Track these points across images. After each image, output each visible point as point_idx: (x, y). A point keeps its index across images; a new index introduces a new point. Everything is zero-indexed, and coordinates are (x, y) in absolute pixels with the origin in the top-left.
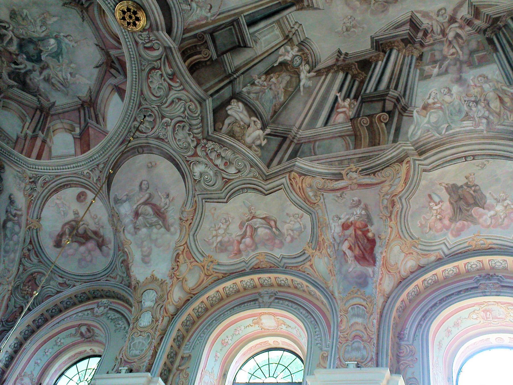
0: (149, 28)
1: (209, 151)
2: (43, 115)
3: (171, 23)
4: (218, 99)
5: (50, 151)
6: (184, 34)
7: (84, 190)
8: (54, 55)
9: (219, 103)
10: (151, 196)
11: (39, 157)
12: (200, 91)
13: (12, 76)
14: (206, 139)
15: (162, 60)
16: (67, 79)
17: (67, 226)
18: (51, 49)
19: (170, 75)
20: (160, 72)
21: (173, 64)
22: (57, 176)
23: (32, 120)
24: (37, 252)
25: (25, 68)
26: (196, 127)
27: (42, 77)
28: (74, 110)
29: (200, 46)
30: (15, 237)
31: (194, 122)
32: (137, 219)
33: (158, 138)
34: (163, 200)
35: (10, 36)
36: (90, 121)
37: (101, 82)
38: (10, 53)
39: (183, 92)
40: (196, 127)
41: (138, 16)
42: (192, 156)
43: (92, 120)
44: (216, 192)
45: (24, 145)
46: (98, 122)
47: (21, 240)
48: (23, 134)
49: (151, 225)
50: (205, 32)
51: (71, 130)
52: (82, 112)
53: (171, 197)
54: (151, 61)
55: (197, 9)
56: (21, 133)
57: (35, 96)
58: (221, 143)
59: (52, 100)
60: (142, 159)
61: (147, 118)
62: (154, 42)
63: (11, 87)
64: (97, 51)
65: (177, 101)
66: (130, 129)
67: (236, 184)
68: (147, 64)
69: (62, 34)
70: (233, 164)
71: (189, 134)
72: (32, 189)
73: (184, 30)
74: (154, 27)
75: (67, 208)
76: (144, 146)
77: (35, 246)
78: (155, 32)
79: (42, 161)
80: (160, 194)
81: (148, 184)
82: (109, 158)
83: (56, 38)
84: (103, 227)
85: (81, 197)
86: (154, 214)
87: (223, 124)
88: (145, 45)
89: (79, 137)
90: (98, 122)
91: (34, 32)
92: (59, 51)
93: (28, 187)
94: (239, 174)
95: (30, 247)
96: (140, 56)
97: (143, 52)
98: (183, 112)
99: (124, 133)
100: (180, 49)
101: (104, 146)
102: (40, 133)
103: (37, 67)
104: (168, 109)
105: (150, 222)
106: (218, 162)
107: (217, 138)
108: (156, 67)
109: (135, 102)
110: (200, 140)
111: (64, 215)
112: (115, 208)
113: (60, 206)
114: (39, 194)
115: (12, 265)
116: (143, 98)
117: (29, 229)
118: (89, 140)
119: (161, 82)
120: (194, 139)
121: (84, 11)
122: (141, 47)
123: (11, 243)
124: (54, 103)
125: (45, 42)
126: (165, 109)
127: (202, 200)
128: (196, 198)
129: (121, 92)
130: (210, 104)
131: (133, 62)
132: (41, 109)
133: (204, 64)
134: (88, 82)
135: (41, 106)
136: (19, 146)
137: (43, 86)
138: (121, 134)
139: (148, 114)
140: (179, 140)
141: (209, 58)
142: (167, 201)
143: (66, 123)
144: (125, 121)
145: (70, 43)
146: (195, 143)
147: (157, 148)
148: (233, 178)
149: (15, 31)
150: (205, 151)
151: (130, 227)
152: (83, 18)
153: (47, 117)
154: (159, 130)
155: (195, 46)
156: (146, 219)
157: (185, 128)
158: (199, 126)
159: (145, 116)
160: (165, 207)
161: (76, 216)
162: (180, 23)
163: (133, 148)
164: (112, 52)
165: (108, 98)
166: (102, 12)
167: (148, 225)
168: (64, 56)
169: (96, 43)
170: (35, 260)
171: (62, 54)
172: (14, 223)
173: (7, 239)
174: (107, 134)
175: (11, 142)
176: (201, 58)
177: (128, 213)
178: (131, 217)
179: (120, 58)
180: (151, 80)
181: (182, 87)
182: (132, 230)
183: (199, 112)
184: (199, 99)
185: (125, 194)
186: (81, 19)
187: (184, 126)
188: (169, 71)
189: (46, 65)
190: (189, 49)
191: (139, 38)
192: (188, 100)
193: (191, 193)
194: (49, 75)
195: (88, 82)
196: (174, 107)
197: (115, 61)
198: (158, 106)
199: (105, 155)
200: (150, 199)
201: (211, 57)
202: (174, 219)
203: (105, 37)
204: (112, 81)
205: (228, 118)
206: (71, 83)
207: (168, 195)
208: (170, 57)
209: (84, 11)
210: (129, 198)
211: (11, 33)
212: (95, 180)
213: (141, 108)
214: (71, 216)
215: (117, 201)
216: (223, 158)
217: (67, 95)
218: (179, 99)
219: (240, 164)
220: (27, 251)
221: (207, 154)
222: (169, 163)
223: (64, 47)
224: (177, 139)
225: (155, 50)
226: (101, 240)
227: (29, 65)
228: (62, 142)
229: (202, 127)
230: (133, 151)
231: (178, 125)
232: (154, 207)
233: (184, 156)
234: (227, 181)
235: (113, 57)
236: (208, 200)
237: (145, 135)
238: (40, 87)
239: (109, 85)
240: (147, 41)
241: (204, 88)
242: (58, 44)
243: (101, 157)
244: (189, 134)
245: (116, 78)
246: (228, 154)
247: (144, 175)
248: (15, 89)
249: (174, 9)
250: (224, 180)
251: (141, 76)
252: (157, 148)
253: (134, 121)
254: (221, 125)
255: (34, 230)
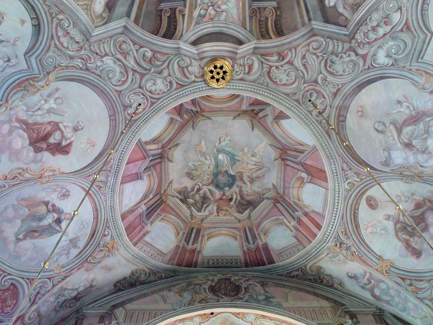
0: (233, 62)
1: (366, 39)
2: (281, 202)
3: (233, 37)
4: (315, 14)
5: (316, 212)
6: (246, 29)
7: (364, 197)
8: (233, 162)
9: (319, 13)
10: (393, 123)
11: (319, 227)
12: (303, 31)
13: (241, 210)
14: (351, 40)
15: (263, 61)
16: (256, 162)
17: (400, 234)
18: (227, 161)
19: (279, 59)
20: (274, 68)
21: (269, 51)
22: (342, 219)
23: (283, 215)
24: (417, 278)
25: (236, 194)
26: (336, 47)
27: (248, 184)
28: (285, 168)
29: (261, 16)
30: (392, 292)
31: (330, 48)
32: (414, 146)
33: (335, 94)
34: (402, 110)
35: (207, 189)
36: (299, 159)
37: (267, 131)
38: (221, 199)
39: (298, 50)
40: (336, 47)
41: (219, 65)
42: (365, 60)
43: (299, 156)
44: (415, 43)
45: (303, 234)
46: (302, 152)
47: (396, 287)
48: (294, 231)
49: (427, 132)
50: (250, 7)
51: (302, 181)
52: (288, 163)
53: (402, 99)
54: (261, 74)
55: (227, 5)
56: (292, 232)
57: (263, 199)
58: (362, 22)
59: (270, 186)
60: (351, 120)
61: (313, 99)
62: (246, 63)
63: (249, 217)
64: (240, 121)
65: (305, 60)
66: (318, 121)
67: (414, 17)
68: (263, 78)
69: (217, 144)
70: (389, 14)
71: (341, 57)
72: (347, 250)
73: (243, 27)
74: (232, 55)
75: (379, 224)
76: (339, 112)
77: (410, 278)
78: (237, 57)
79: (324, 226)
80: (394, 112)
81: (379, 122)
82: (339, 156)
83: (219, 151)
84: (413, 194)
85: (372, 204)
86: (415, 125)
87: (342, 15)
88: (246, 72)
89: (310, 177)
90: (302, 152)
91: (209, 168)
92: (231, 156)
93: (344, 252)
94: (404, 9)
95: (408, 282)
96: (254, 82)
97: (252, 77)
98: (318, 57)
99: (319, 129)
100: (258, 39)
101: (326, 155)
102: (296, 213)
103: (238, 183)
104: (310, 73)
105: (422, 132)
106: (381, 31)
107: (355, 26)
108: (268, 70)
109: (295, 106)
110: (351, 47)
111: (386, 231)
112: (393, 168)
113: (375, 230)
114: (355, 245)
115: (420, 311)
116: (293, 96)
117: (387, 273)
118: (317, 168)
119: (283, 71)
120: (348, 53)
121: (203, 114)
122: (246, 77)
123: (396, 299)
124: (273, 185)
125: (220, 164)
126: (309, 76)
127: (417, 62)
128: (413, 68)
129: (281, 116)
130: (318, 25)
131: (258, 91)
132: (276, 201)
133: (278, 18)
134: (264, 143)
135: (273, 199)
136: (304, 241)
137: (256, 187)
138: (320, 133)
139: (309, 96)
140: (344, 71)
141: (274, 11)
142: (405, 104)
143: (294, 184)
144: (309, 123)
145: (226, 142)
146: (352, 53)
147: (345, 99)
148: (405, 18)
149: (204, 183)
150: (364, 44)
151: (420, 157)
152: (209, 118)
153: (284, 199)
154: (328, 91)
155: (260, 21)
156: (417, 136)
157: (333, 61)
158: (336, 44)
159: (310, 101)
160: (412, 108)
161: (391, 218)
162: (236, 28)
163: (338, 125)
164: (244, 107)
165: (283, 131)
166: (208, 98)
167: (425, 136)
168: (236, 154)
169: (232, 118)
170: (425, 285)
171: (234, 154)
172: (377, 287)
173: (391, 302)
174: (316, 147)
175: (298, 247)
176: (272, 19)
177: (404, 156)
178: (410, 153)
179: (251, 102)
180: (278, 81)
181: (293, 50)
182: (425, 156)
183: (322, 39)
184: (309, 35)
185: (382, 152)
186: (209, 121)
187: (332, 61)
188: (275, 58)
189: (239, 174)
190: (260, 28)
191: (238, 75)
192: (307, 48)
193: (405, 73)
194: (249, 177)
195: (264, 143)
196: (309, 65)
197: (253, 108)
198: (304, 83)
199: (336, 158)
200: (397, 124)
201: (274, 8)
202: (429, 100)
203: (229, 107)
204: (269, 119)
205: (337, 7)
206: (260, 160)
207: (399, 102)
208: (263, 51)
209: (203, 114)
210: (388, 149)
211: (204, 187)
212: (357, 179)
213: (301, 102)
214: (390, 225)
215: (386, 163)
216: (377, 25)
217: (270, 169)
218: (304, 57)
219: (391, 6)
220: (411, 287)
221: (368, 43)
222: (364, 91)
223: (228, 149)
224: (342, 73)
225: (252, 64)
226: (428, 203)
227: (235, 189)
228: (311, 196)
229: (338, 40)
230: (340, 126)
231: (328, 68)
232: (406, 123)
233: (362, 71)
234: (407, 26)
235: (248, 109)
236: (421, 54)
237: (328, 108)
238: (256, 191)
239: (272, 125)
240: (243, 69)
241: (300, 25)
242: (224, 153)
243: (336, 163)
244: (341, 57)
245: (267, 115)
246: (376, 17)
247: (368, 124)
248: (252, 214)
249: (223, 29)
250: (404, 30)
251: (271, 88)
252: (345, 99)
253: (311, 114)
254: (342, 17)
255: (390, 269)
